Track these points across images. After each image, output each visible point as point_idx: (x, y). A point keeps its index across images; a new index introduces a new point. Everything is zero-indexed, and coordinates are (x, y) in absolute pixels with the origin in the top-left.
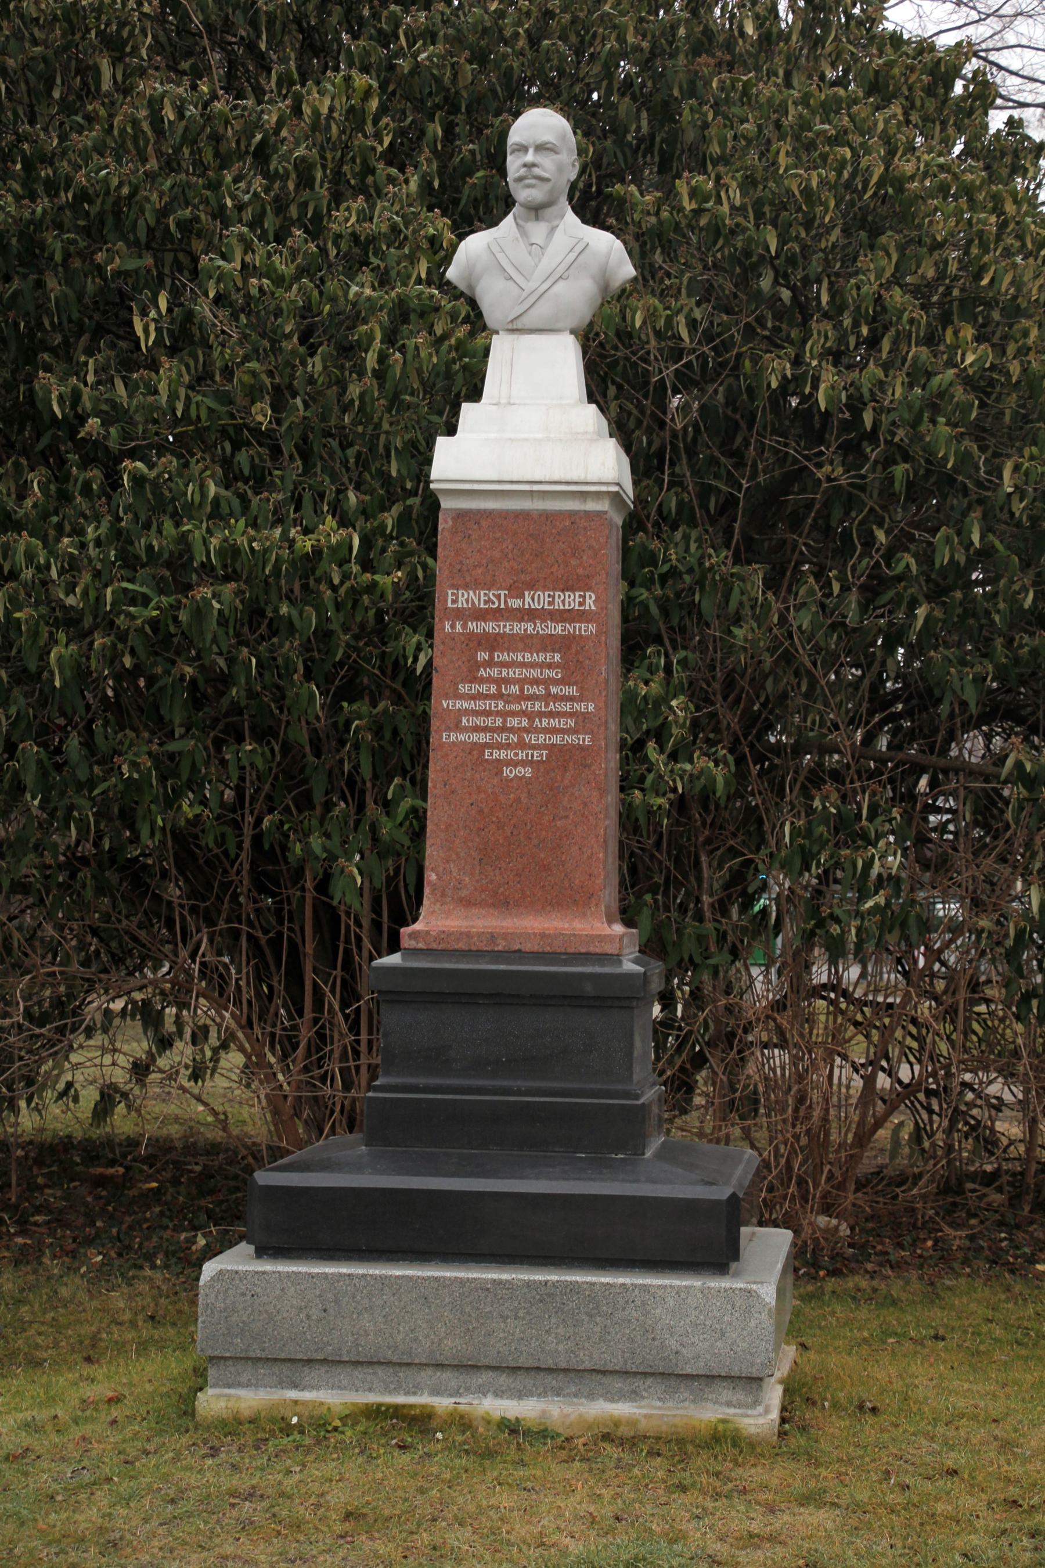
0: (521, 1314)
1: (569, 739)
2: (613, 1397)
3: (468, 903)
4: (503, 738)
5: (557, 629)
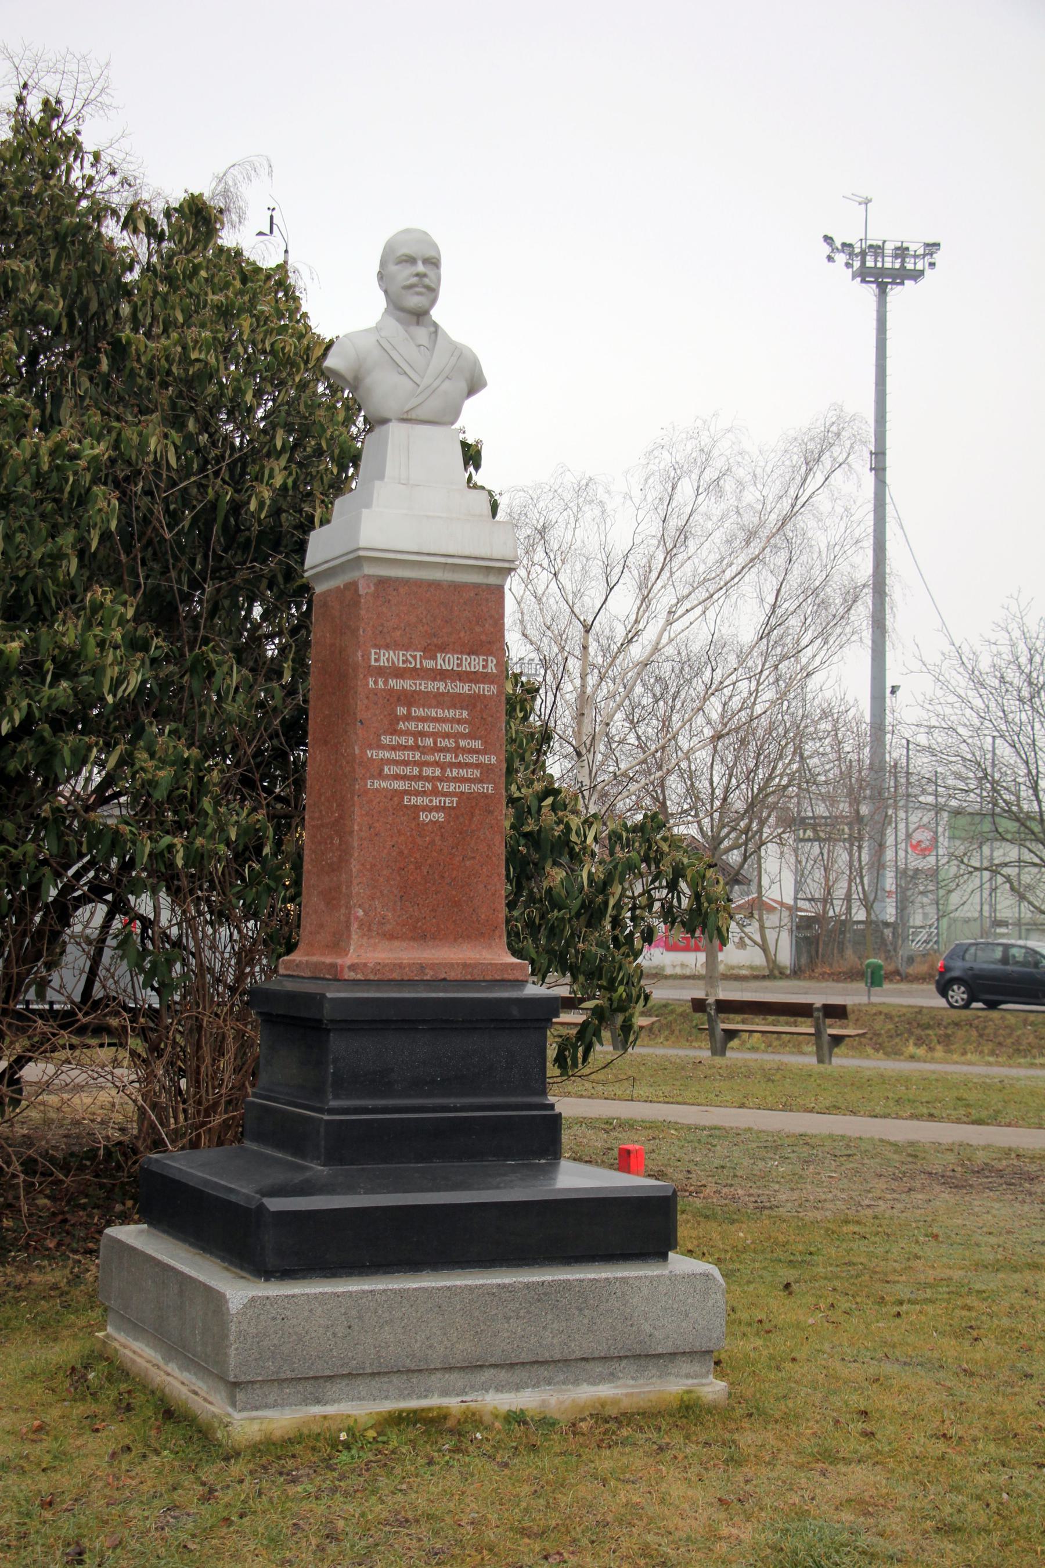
0: (522, 1314)
1: (476, 788)
2: (596, 1380)
3: (391, 937)
4: (419, 786)
5: (464, 688)
